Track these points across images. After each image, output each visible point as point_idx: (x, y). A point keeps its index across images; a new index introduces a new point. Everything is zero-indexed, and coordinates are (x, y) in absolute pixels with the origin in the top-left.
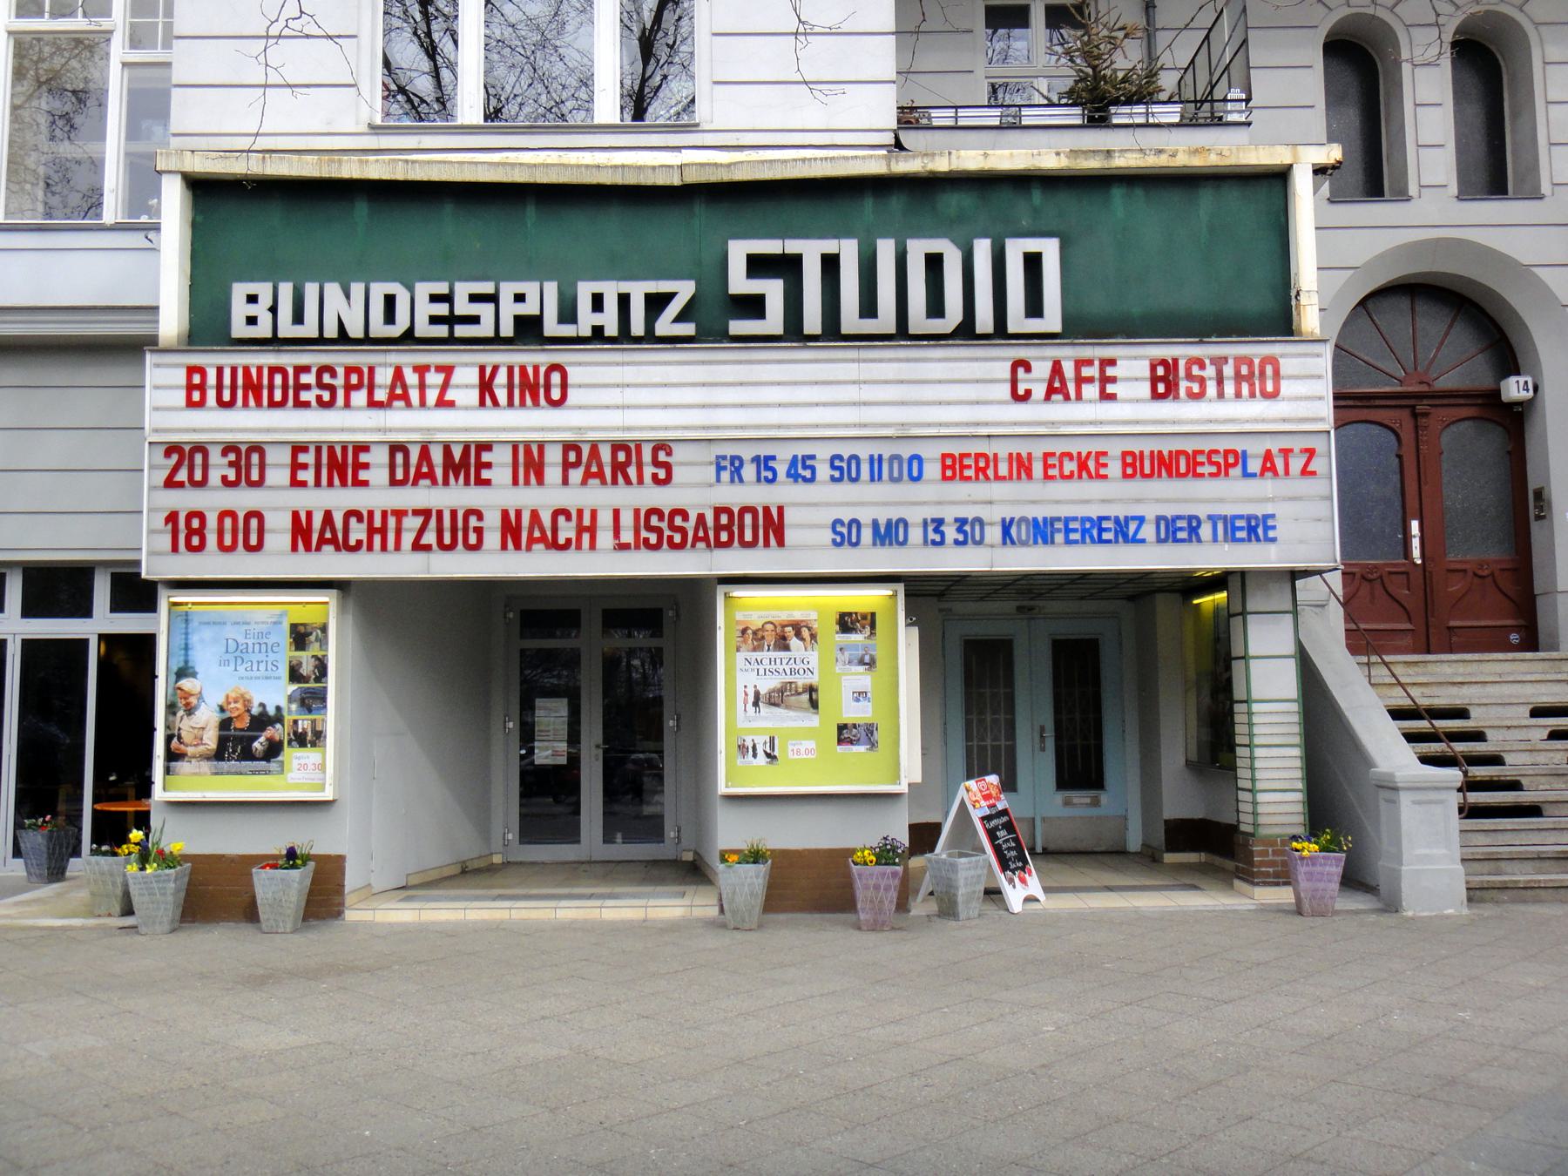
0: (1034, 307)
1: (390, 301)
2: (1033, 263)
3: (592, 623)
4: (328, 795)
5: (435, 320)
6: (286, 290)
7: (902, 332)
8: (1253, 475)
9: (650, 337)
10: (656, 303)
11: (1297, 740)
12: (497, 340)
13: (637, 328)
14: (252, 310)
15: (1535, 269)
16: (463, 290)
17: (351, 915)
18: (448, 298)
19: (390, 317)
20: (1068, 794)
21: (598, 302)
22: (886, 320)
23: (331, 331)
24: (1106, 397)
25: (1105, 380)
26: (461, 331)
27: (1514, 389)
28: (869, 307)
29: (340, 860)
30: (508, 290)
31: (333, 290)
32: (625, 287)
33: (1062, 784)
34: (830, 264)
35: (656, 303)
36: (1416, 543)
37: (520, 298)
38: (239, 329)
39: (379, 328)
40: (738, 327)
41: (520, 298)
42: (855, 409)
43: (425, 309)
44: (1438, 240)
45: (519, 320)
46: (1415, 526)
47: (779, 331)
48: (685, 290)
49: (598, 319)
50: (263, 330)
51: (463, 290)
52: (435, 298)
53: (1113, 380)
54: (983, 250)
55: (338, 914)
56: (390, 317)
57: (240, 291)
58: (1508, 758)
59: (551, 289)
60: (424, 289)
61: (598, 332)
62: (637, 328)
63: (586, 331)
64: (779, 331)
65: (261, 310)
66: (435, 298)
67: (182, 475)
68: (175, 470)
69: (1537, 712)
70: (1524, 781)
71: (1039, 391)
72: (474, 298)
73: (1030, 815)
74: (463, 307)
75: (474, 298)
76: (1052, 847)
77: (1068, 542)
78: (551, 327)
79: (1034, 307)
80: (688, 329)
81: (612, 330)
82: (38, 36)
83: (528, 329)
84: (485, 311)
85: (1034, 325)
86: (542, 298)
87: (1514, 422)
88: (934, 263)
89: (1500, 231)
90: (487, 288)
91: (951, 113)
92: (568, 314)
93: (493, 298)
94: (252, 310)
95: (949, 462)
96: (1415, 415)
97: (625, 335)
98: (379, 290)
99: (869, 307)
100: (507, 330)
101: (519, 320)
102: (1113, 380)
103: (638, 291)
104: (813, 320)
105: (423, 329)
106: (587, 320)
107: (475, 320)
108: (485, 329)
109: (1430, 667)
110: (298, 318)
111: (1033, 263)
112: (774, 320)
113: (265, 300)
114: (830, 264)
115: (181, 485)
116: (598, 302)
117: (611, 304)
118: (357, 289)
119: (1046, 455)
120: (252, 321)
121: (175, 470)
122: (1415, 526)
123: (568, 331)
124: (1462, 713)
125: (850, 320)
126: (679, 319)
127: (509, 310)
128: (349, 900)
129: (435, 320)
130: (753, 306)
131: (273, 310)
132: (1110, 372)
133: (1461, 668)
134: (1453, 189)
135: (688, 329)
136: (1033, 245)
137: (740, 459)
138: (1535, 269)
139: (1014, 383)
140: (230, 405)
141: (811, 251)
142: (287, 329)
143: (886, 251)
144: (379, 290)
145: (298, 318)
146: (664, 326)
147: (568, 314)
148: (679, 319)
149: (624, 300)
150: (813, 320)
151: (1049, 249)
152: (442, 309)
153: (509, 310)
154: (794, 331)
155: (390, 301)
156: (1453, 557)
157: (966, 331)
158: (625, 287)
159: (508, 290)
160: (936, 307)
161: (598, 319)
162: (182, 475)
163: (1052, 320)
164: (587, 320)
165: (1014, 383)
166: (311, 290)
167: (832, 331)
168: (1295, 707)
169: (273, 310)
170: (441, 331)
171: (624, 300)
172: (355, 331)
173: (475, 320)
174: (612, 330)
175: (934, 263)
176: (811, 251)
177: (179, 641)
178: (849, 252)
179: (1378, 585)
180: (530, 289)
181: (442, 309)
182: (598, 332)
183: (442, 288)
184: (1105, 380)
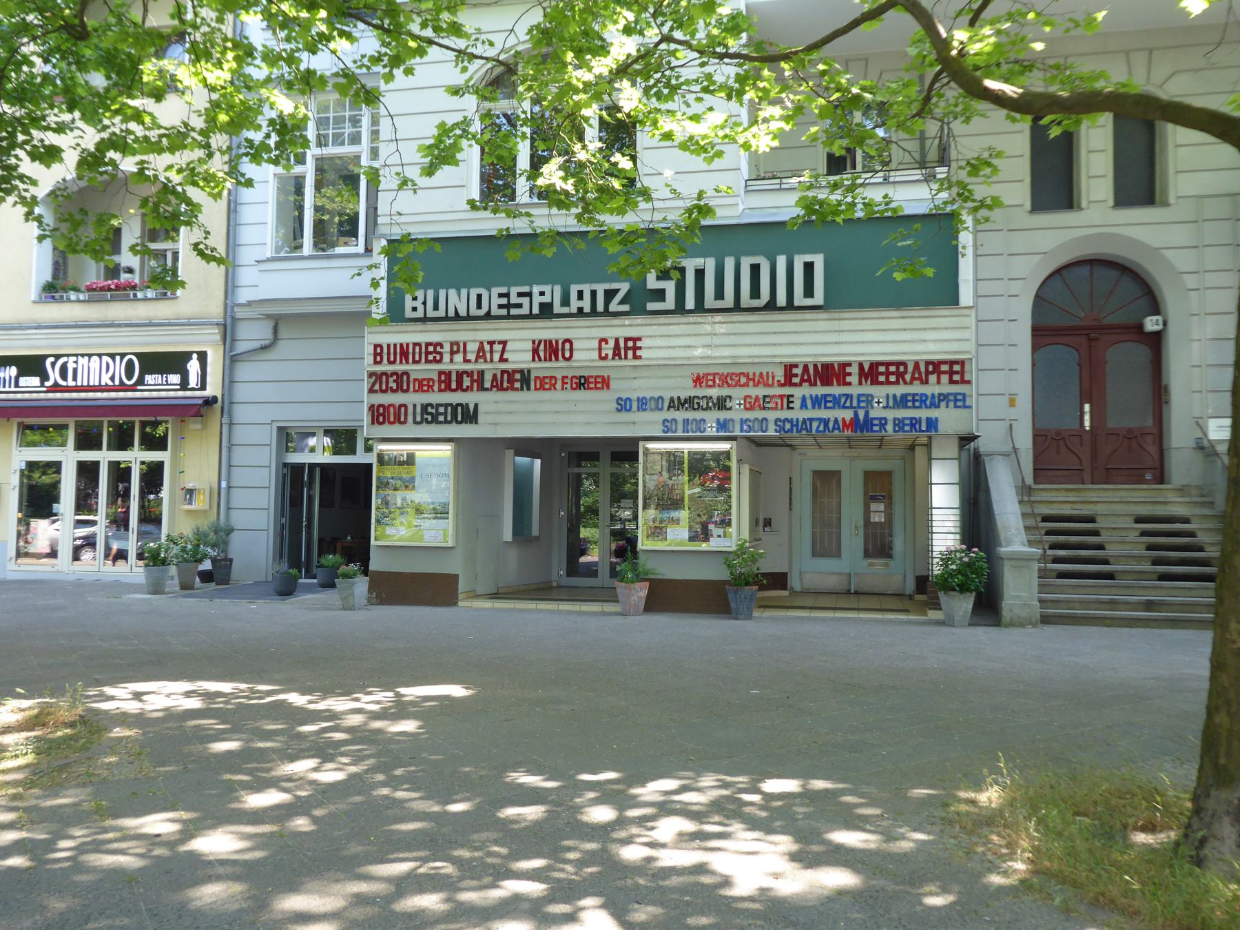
0: (809, 292)
1: (479, 297)
2: (809, 267)
3: (605, 458)
4: (450, 544)
5: (500, 306)
6: (430, 293)
7: (737, 307)
9: (607, 313)
10: (610, 295)
11: (958, 530)
12: (531, 316)
13: (600, 308)
14: (415, 304)
15: (1165, 252)
16: (514, 291)
17: (460, 604)
18: (507, 295)
19: (479, 306)
20: (871, 561)
21: (580, 295)
22: (729, 300)
23: (451, 313)
26: (514, 312)
27: (1151, 324)
28: (719, 295)
29: (457, 576)
30: (536, 290)
31: (452, 292)
32: (594, 287)
33: (867, 554)
34: (700, 273)
35: (610, 295)
36: (1087, 418)
37: (542, 294)
38: (409, 314)
39: (474, 311)
40: (651, 306)
41: (542, 294)
43: (496, 301)
44: (1099, 234)
45: (542, 305)
46: (1087, 407)
47: (673, 307)
48: (624, 287)
49: (580, 304)
50: (420, 314)
51: (514, 291)
52: (501, 295)
54: (781, 261)
55: (455, 604)
56: (479, 306)
57: (408, 298)
58: (1107, 547)
59: (558, 290)
60: (495, 291)
61: (580, 310)
62: (600, 308)
63: (574, 310)
64: (673, 307)
65: (418, 304)
66: (501, 295)
67: (377, 387)
68: (374, 384)
69: (1139, 520)
70: (1111, 560)
72: (520, 295)
73: (847, 571)
74: (514, 299)
75: (520, 295)
76: (860, 590)
77: (956, 406)
78: (557, 309)
79: (809, 292)
80: (626, 308)
81: (587, 309)
82: (331, 159)
83: (546, 311)
84: (525, 301)
85: (809, 302)
86: (552, 294)
87: (1156, 341)
88: (755, 269)
90: (526, 289)
91: (778, 181)
92: (566, 302)
93: (529, 295)
94: (415, 304)
96: (1090, 340)
97: (594, 312)
98: (474, 292)
99: (719, 295)
100: (536, 310)
101: (542, 305)
103: (601, 289)
104: (690, 303)
105: (495, 311)
106: (575, 304)
107: (520, 306)
108: (525, 310)
109: (1082, 494)
110: (436, 308)
111: (809, 267)
112: (670, 303)
113: (421, 299)
114: (700, 273)
115: (376, 391)
116: (580, 295)
117: (587, 296)
118: (464, 292)
120: (414, 309)
121: (374, 384)
122: (1087, 407)
123: (565, 310)
124: (1091, 520)
125: (710, 300)
126: (621, 303)
127: (537, 300)
128: (460, 596)
129: (500, 306)
130: (660, 295)
131: (424, 303)
133: (1102, 494)
134: (1111, 202)
135: (626, 308)
136: (808, 258)
138: (1165, 252)
140: (415, 344)
141: (691, 265)
142: (431, 313)
143: (729, 263)
144: (474, 292)
145: (436, 308)
146: (614, 307)
147: (566, 302)
148: (621, 303)
149: (594, 293)
150: (690, 303)
151: (819, 261)
152: (504, 301)
153: (537, 300)
154: (680, 309)
155: (479, 297)
156: (1111, 424)
157: (771, 306)
158: (594, 287)
159: (536, 290)
160: (755, 293)
161: (580, 304)
162: (377, 387)
163: (819, 298)
164: (575, 304)
166: (442, 293)
167: (700, 308)
168: (957, 512)
169: (424, 303)
170: (504, 312)
171: (594, 293)
172: (463, 313)
173: (520, 306)
174: (587, 309)
175: (755, 269)
176: (691, 265)
178: (710, 265)
179: (1061, 443)
180: (547, 289)
181: (504, 301)
182: (580, 310)
183: (504, 290)
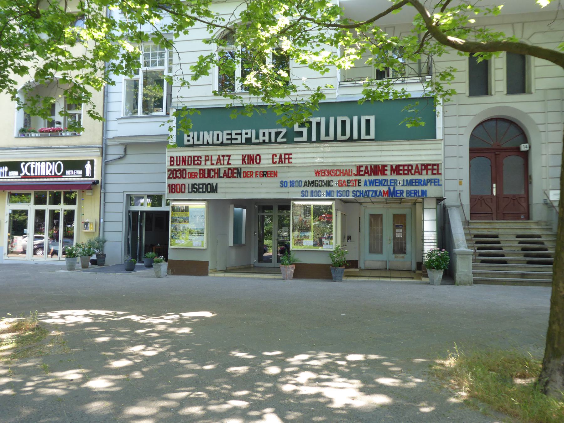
0: (368, 133)
1: (218, 135)
2: (368, 121)
4: (205, 248)
5: (228, 139)
6: (196, 133)
7: (335, 140)
8: (221, 177)
9: (276, 142)
10: (277, 134)
11: (436, 241)
12: (241, 144)
13: (273, 140)
14: (189, 138)
15: (530, 115)
16: (234, 132)
17: (209, 275)
18: (231, 134)
19: (218, 139)
20: (396, 255)
21: (264, 134)
22: (331, 137)
23: (205, 143)
24: (289, 162)
25: (289, 158)
26: (234, 142)
27: (524, 147)
28: (327, 134)
29: (208, 262)
30: (244, 132)
31: (206, 133)
32: (270, 130)
33: (394, 252)
34: (318, 124)
35: (277, 134)
36: (494, 190)
37: (247, 134)
38: (186, 143)
39: (216, 142)
40: (296, 139)
41: (247, 134)
42: (393, 154)
43: (226, 137)
44: (500, 107)
45: (246, 139)
46: (494, 185)
47: (306, 140)
48: (284, 131)
49: (264, 138)
50: (191, 143)
51: (234, 132)
52: (228, 134)
53: (291, 158)
54: (355, 119)
55: (207, 275)
56: (218, 139)
57: (186, 135)
58: (504, 249)
59: (254, 132)
60: (225, 132)
61: (264, 141)
62: (273, 140)
63: (261, 141)
64: (306, 140)
65: (190, 138)
66: (228, 134)
67: (171, 176)
68: (170, 175)
69: (518, 236)
71: (278, 161)
72: (236, 134)
73: (385, 260)
74: (234, 136)
75: (236, 134)
76: (391, 268)
78: (254, 140)
79: (368, 133)
80: (285, 140)
81: (267, 141)
82: (151, 72)
83: (248, 141)
84: (239, 137)
85: (368, 137)
86: (251, 134)
87: (526, 155)
88: (343, 122)
89: (518, 105)
90: (239, 131)
91: (354, 82)
92: (257, 137)
93: (241, 134)
94: (189, 138)
95: (410, 168)
96: (496, 155)
97: (270, 142)
98: (216, 133)
99: (327, 134)
100: (244, 141)
101: (246, 139)
102: (291, 158)
103: (273, 131)
104: (314, 138)
105: (225, 142)
106: (261, 138)
107: (236, 139)
108: (239, 141)
109: (492, 225)
110: (198, 140)
111: (368, 121)
112: (305, 138)
113: (191, 136)
114: (318, 124)
115: (171, 178)
116: (264, 134)
117: (267, 135)
118: (211, 133)
119: (256, 172)
120: (189, 141)
121: (170, 175)
122: (494, 185)
123: (257, 141)
124: (496, 236)
125: (323, 137)
126: (282, 138)
127: (244, 136)
128: (209, 271)
129: (228, 139)
130: (300, 134)
131: (193, 138)
132: (290, 156)
133: (501, 225)
134: (505, 92)
135: (285, 140)
136: (368, 117)
137: (253, 172)
138: (530, 115)
139: (273, 159)
141: (314, 120)
142: (196, 142)
143: (332, 120)
144: (216, 133)
145: (198, 140)
146: (279, 140)
147: (257, 137)
148: (282, 138)
149: (270, 133)
150: (314, 138)
151: (372, 119)
152: (229, 137)
153: (244, 136)
154: (309, 140)
155: (218, 135)
157: (351, 139)
158: (270, 130)
159: (244, 132)
160: (344, 133)
161: (264, 138)
162: (171, 176)
163: (372, 136)
164: (261, 138)
165: (273, 159)
166: (201, 133)
167: (318, 140)
168: (435, 233)
169: (193, 138)
170: (229, 142)
171: (270, 133)
172: (210, 142)
173: (236, 139)
174: (267, 141)
175: (343, 122)
176: (314, 120)
177: (490, 275)
178: (323, 121)
179: (483, 201)
180: (249, 131)
181: (229, 137)
182: (264, 141)
183: (229, 132)
184: (289, 158)
